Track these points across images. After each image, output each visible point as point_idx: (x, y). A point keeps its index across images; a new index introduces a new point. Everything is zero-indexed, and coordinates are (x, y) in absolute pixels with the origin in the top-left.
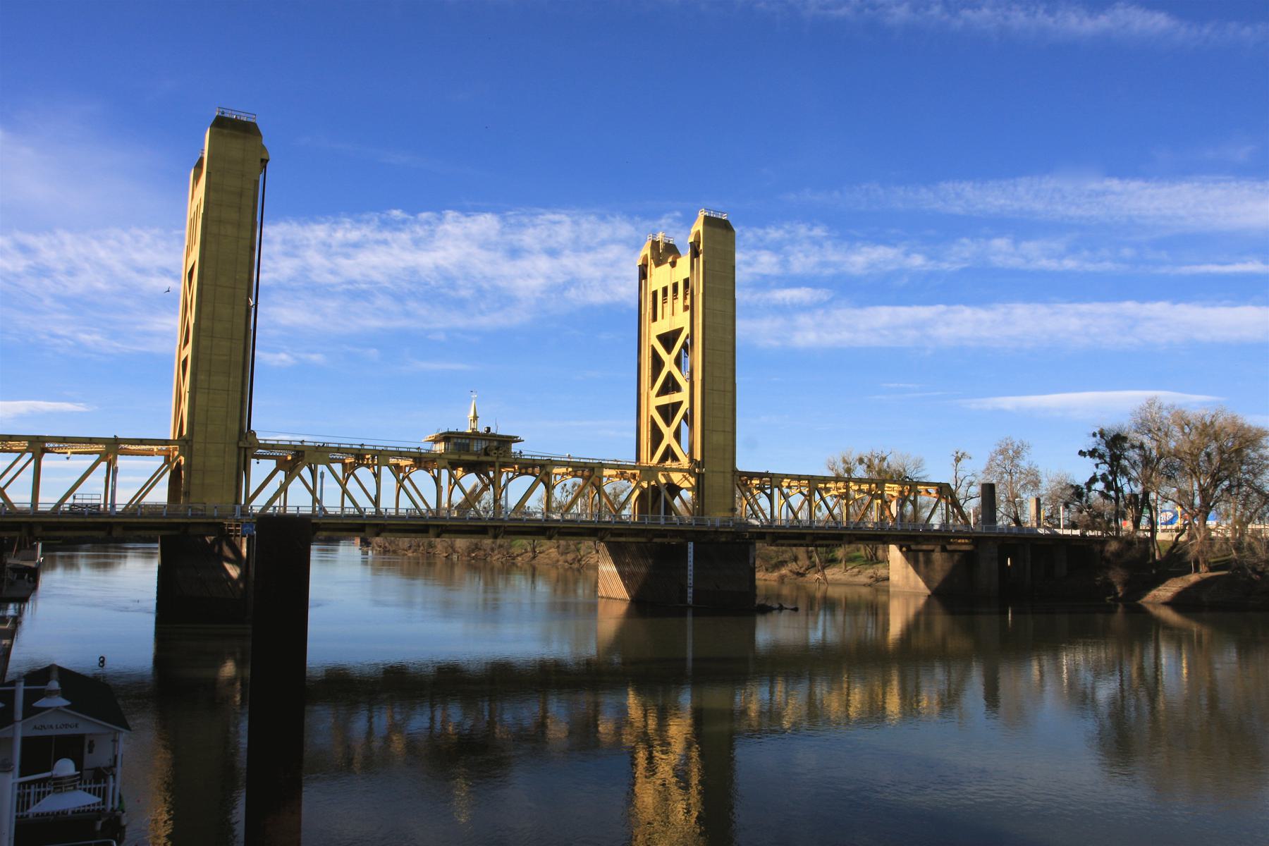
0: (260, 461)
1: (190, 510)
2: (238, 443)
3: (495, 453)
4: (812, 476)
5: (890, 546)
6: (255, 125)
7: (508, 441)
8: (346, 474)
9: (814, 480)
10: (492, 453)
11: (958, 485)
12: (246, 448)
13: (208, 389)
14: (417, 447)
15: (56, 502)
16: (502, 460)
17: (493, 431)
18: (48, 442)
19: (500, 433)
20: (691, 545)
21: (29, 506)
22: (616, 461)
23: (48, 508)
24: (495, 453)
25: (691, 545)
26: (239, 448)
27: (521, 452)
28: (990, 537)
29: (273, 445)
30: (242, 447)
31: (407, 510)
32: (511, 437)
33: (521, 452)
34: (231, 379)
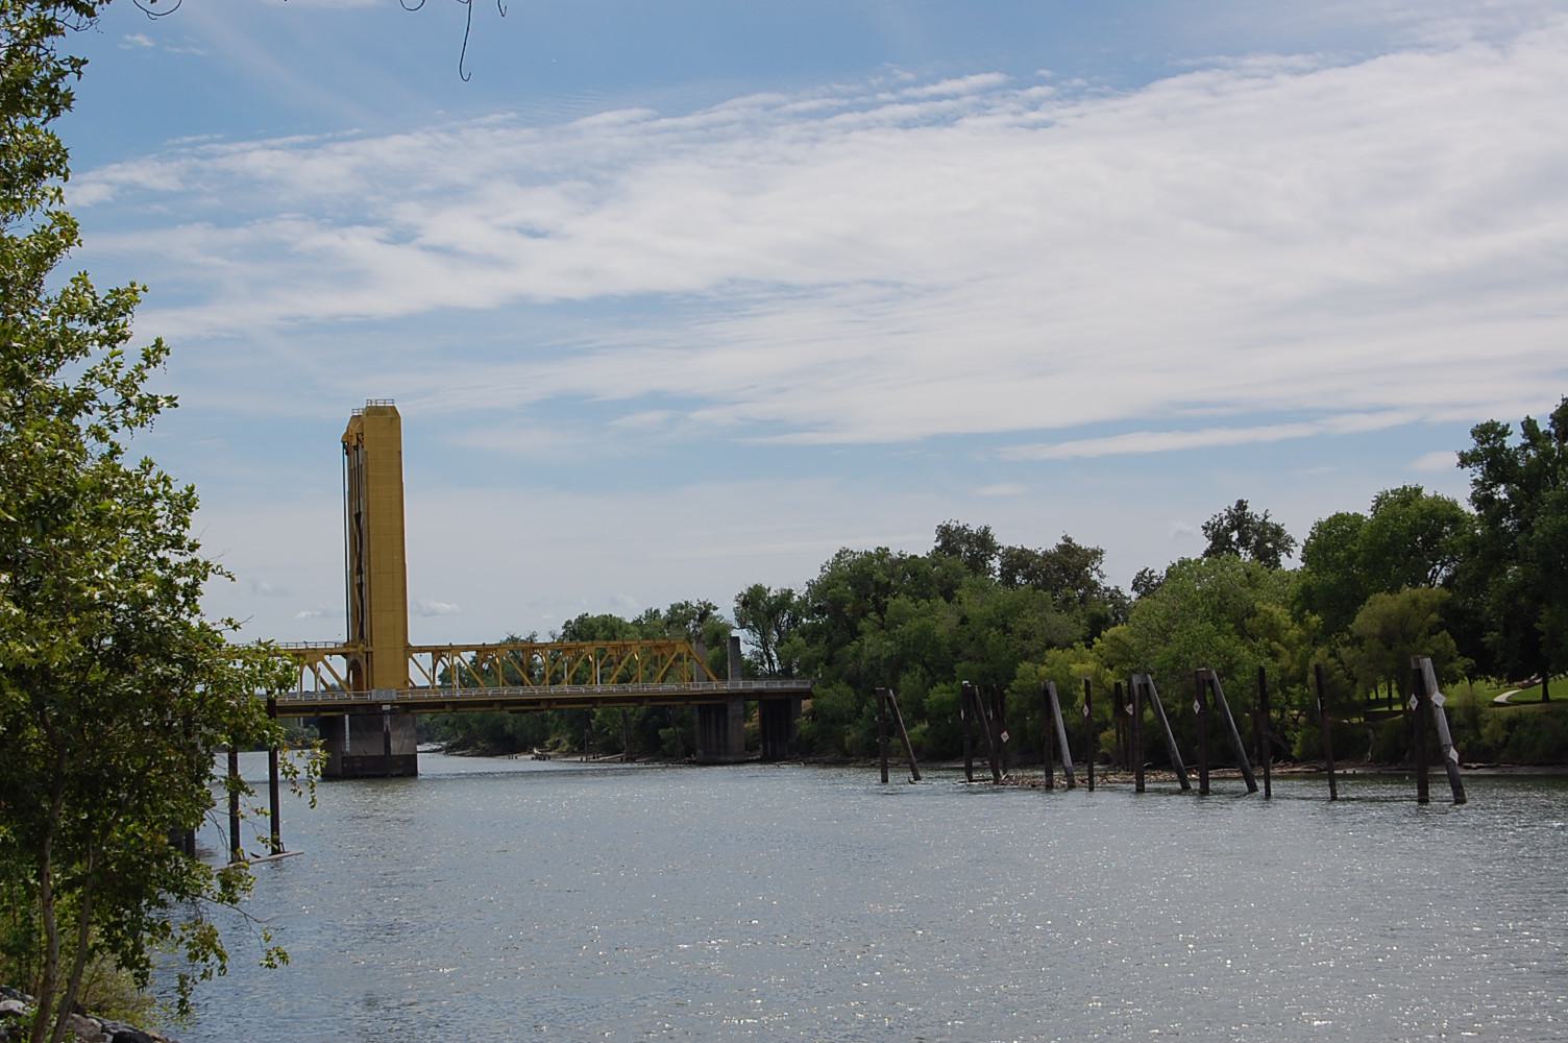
20: (347, 717)
25: (347, 717)
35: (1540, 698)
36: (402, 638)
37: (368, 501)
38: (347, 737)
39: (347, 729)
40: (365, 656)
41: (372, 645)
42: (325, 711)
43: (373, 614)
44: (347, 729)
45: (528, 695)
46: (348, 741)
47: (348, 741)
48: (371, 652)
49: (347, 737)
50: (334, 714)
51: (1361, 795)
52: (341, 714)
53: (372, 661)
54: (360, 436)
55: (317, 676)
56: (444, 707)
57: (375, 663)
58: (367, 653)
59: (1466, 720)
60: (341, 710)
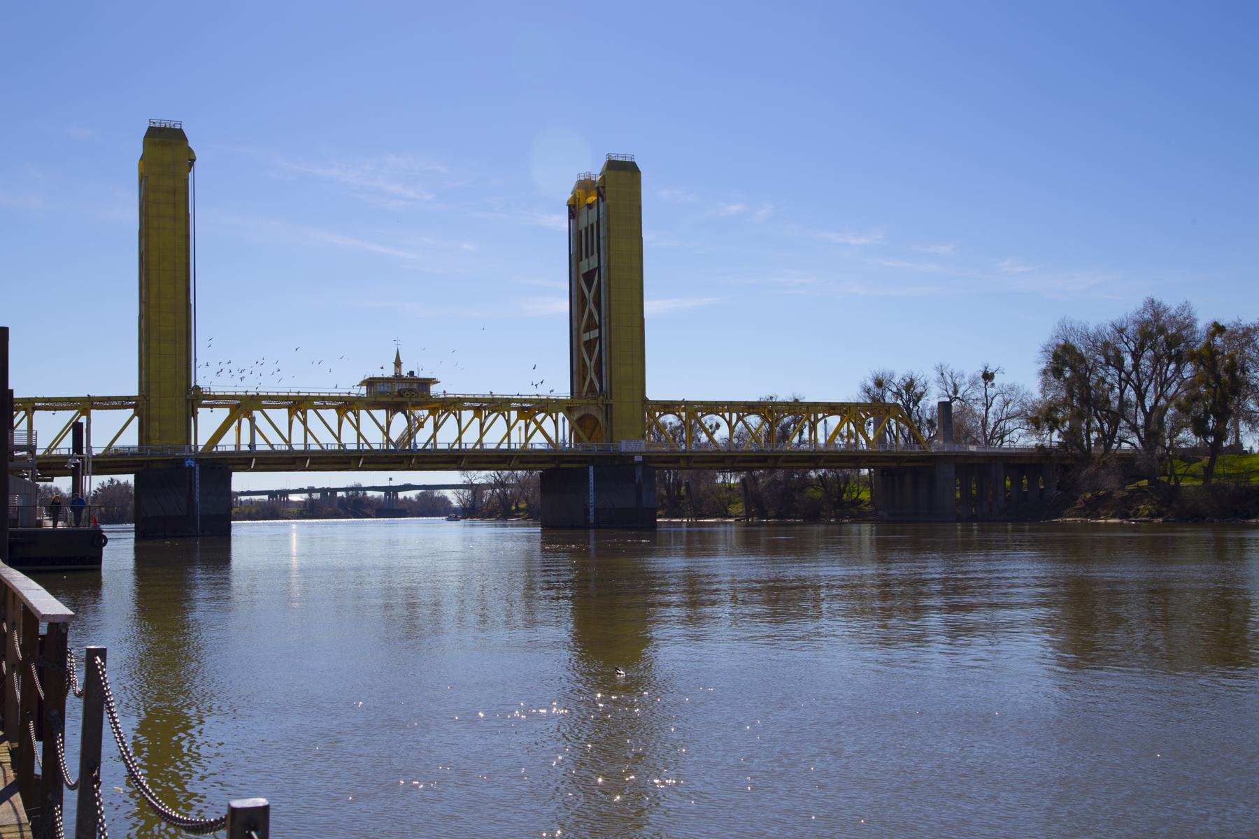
0: (214, 409)
1: (149, 451)
2: (186, 396)
3: (408, 395)
4: (731, 402)
5: (71, 478)
6: (634, 163)
7: (427, 383)
8: (437, 416)
9: (734, 405)
10: (404, 394)
11: (989, 405)
12: (193, 400)
13: (160, 354)
14: (245, 390)
15: (204, 444)
16: (414, 400)
17: (416, 374)
18: (37, 402)
19: (420, 377)
20: (591, 468)
21: (137, 449)
22: (518, 395)
23: (100, 451)
24: (408, 395)
25: (591, 468)
26: (187, 400)
27: (445, 392)
28: (939, 456)
29: (274, 396)
30: (189, 400)
31: (449, 444)
32: (428, 379)
33: (445, 392)
34: (177, 345)
35: (542, 425)
36: (184, 383)
37: (609, 254)
38: (592, 489)
39: (592, 481)
40: (604, 408)
41: (611, 398)
42: (564, 462)
43: (613, 366)
44: (592, 481)
45: (961, 450)
46: (592, 493)
47: (592, 493)
48: (611, 405)
49: (592, 489)
50: (574, 466)
51: (915, 671)
52: (585, 465)
53: (611, 415)
54: (601, 190)
55: (307, 430)
56: (350, 463)
57: (614, 415)
58: (607, 405)
59: (416, 500)
60: (585, 462)
